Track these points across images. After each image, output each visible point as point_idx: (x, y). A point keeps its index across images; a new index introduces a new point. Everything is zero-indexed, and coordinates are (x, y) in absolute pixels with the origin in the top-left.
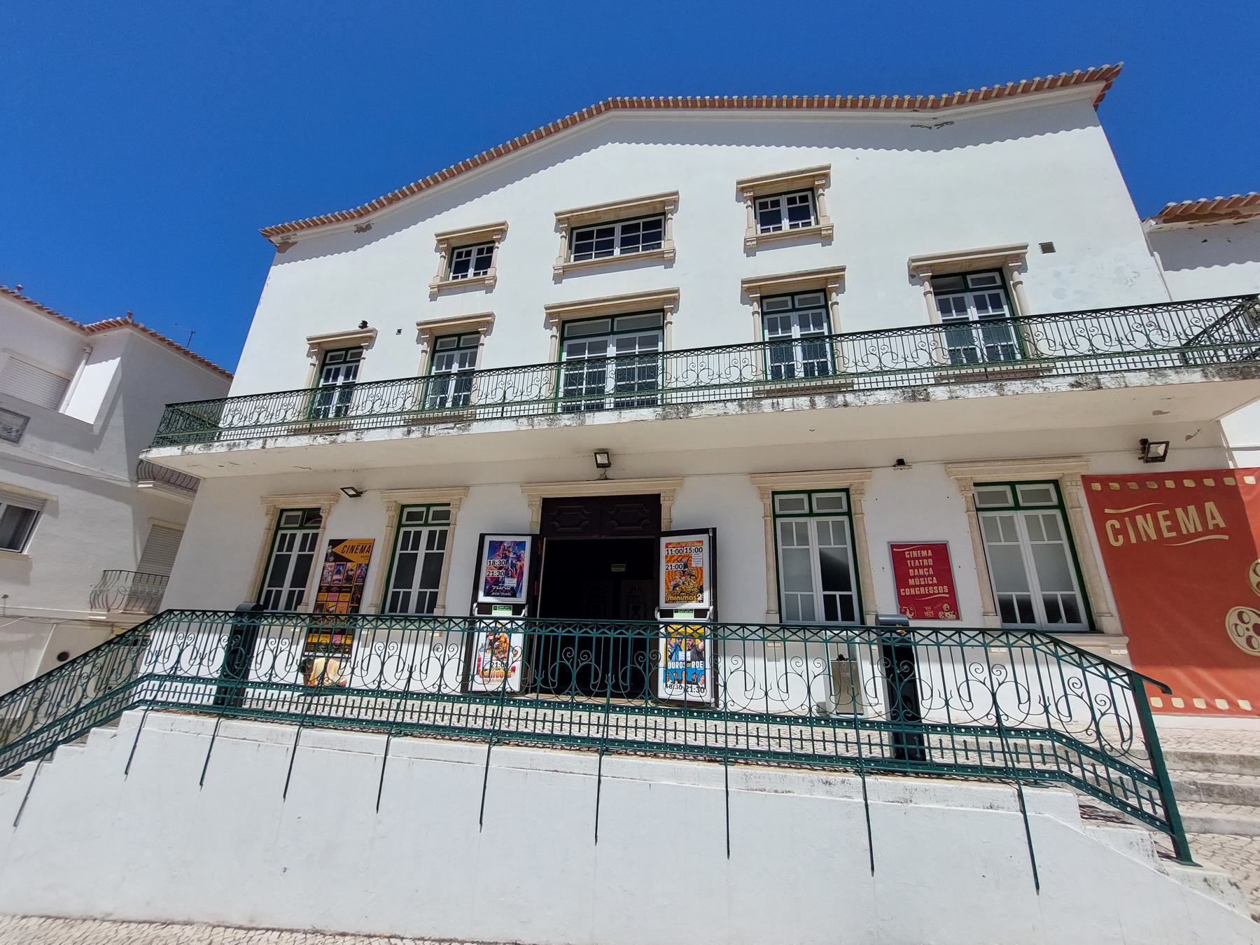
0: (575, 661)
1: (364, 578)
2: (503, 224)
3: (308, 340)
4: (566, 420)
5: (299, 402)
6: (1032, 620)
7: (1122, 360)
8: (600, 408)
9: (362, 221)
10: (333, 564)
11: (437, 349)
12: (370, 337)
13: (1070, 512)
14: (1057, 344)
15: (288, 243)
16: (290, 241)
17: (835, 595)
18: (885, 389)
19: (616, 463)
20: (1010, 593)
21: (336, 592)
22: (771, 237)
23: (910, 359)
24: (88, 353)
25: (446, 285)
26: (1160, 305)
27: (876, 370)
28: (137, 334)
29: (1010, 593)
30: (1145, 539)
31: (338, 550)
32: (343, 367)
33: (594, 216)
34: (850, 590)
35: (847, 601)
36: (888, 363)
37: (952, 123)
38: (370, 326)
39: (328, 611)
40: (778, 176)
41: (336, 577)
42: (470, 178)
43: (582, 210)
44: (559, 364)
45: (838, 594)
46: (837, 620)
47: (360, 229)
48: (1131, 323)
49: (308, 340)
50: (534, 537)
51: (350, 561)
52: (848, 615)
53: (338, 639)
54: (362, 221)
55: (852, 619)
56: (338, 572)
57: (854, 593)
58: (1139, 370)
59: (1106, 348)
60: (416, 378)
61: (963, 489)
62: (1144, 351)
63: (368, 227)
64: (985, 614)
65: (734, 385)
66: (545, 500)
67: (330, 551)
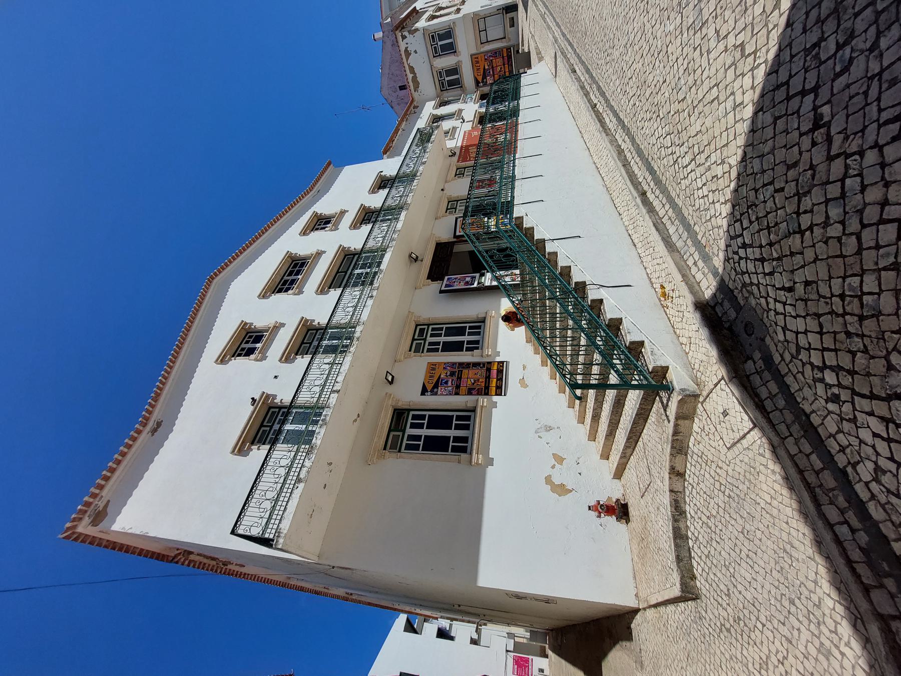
1: (454, 364)
6: (479, 341)
7: (300, 454)
9: (151, 424)
10: (440, 388)
11: (265, 424)
13: (412, 407)
14: (258, 521)
15: (99, 512)
16: (101, 509)
17: (452, 446)
18: (288, 502)
20: (450, 446)
21: (460, 380)
23: (263, 514)
26: (300, 382)
27: (287, 471)
29: (450, 446)
31: (429, 387)
33: (273, 283)
34: (453, 416)
35: (459, 418)
36: (271, 495)
38: (257, 397)
39: (473, 384)
41: (450, 383)
42: (186, 350)
43: (266, 285)
45: (451, 444)
46: (469, 424)
47: (154, 431)
48: (315, 368)
51: (440, 375)
52: (468, 418)
53: (494, 372)
54: (151, 424)
55: (470, 417)
56: (446, 383)
57: (455, 414)
58: (290, 496)
59: (323, 380)
61: (410, 357)
62: (288, 472)
63: (159, 424)
64: (459, 462)
65: (288, 473)
67: (429, 393)
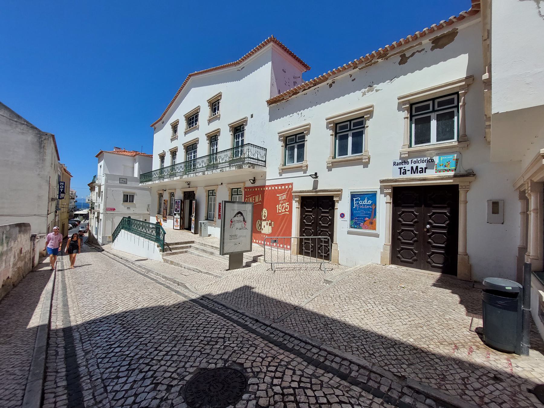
0: (131, 199)
2: (220, 93)
3: (206, 135)
4: (210, 173)
5: (229, 153)
8: (191, 171)
12: (219, 131)
19: (191, 184)
22: (192, 129)
24: (135, 161)
25: (211, 119)
28: (140, 156)
30: (441, 265)
32: (193, 151)
37: (244, 67)
40: (216, 95)
44: (233, 148)
49: (206, 135)
50: (181, 200)
60: (230, 149)
66: (184, 192)
